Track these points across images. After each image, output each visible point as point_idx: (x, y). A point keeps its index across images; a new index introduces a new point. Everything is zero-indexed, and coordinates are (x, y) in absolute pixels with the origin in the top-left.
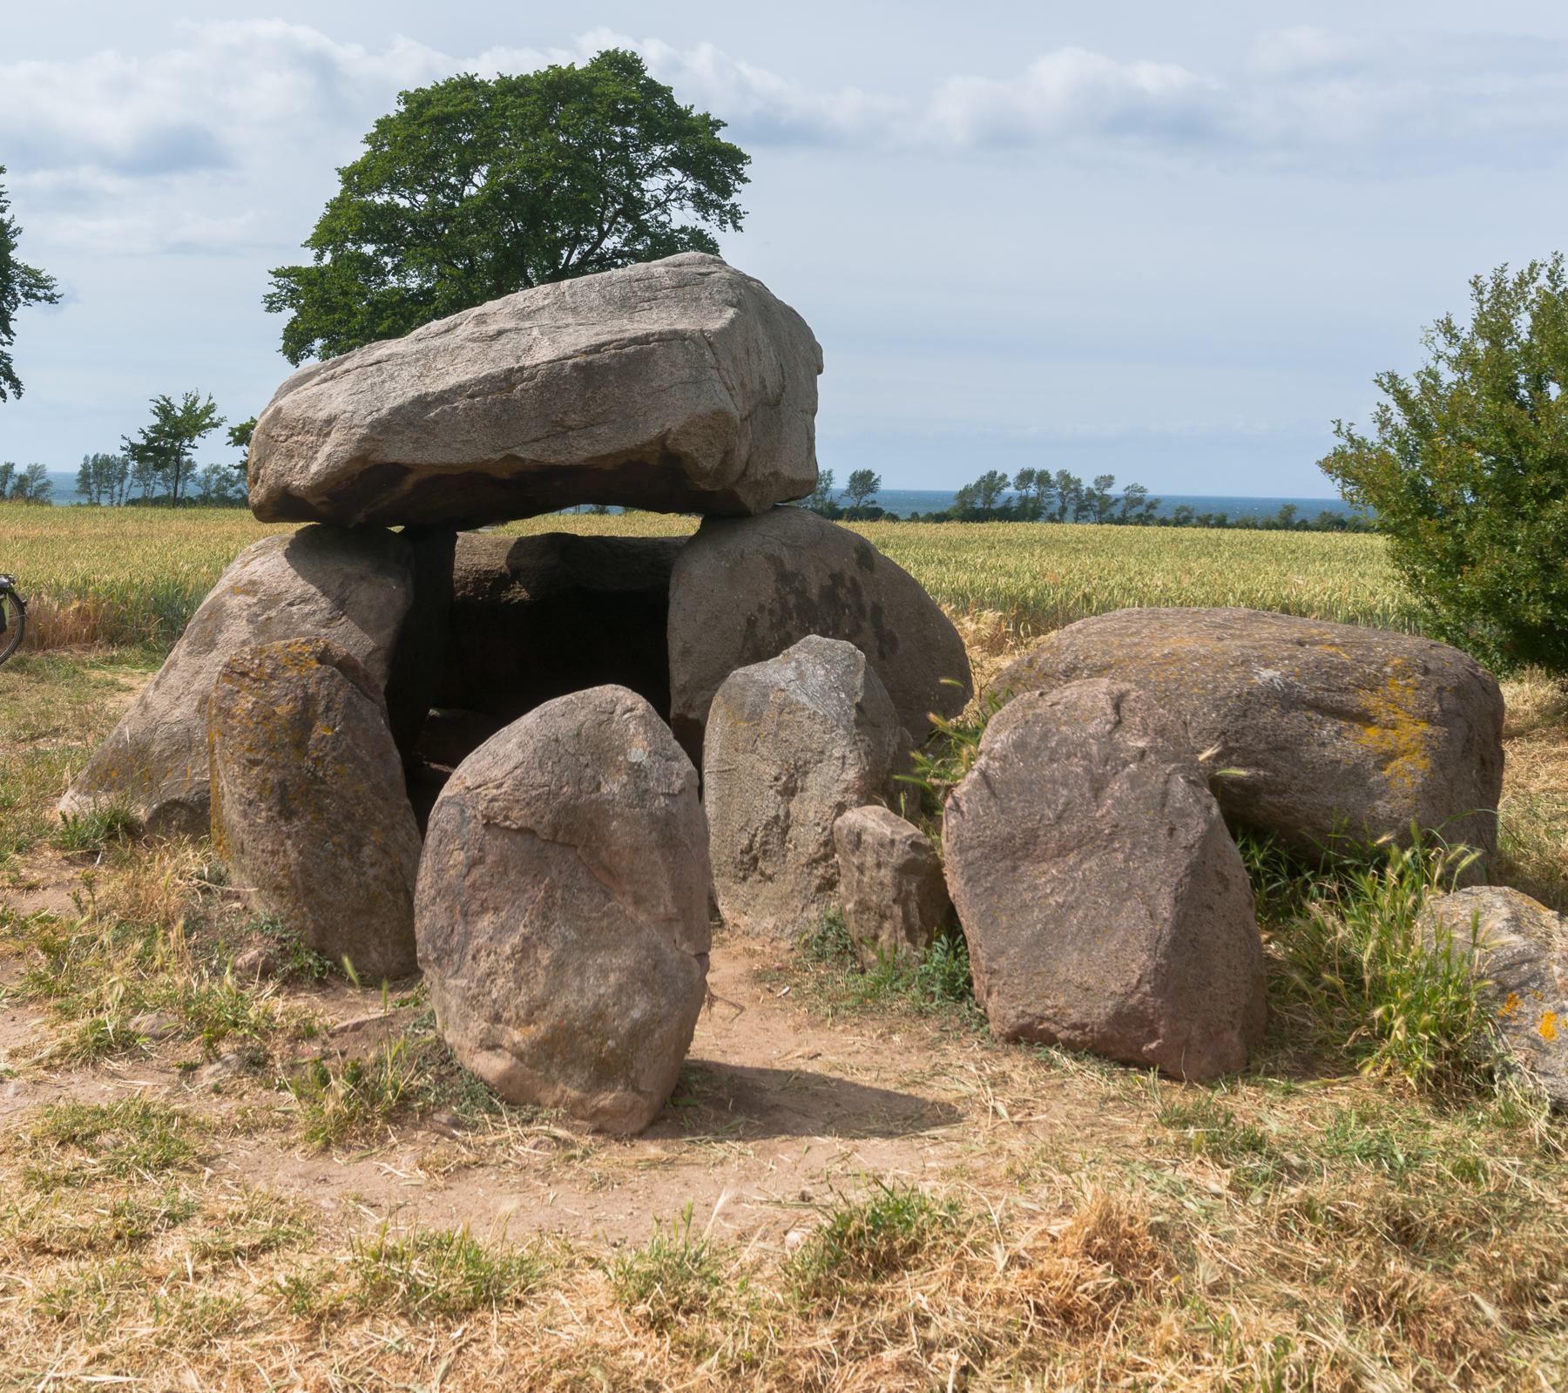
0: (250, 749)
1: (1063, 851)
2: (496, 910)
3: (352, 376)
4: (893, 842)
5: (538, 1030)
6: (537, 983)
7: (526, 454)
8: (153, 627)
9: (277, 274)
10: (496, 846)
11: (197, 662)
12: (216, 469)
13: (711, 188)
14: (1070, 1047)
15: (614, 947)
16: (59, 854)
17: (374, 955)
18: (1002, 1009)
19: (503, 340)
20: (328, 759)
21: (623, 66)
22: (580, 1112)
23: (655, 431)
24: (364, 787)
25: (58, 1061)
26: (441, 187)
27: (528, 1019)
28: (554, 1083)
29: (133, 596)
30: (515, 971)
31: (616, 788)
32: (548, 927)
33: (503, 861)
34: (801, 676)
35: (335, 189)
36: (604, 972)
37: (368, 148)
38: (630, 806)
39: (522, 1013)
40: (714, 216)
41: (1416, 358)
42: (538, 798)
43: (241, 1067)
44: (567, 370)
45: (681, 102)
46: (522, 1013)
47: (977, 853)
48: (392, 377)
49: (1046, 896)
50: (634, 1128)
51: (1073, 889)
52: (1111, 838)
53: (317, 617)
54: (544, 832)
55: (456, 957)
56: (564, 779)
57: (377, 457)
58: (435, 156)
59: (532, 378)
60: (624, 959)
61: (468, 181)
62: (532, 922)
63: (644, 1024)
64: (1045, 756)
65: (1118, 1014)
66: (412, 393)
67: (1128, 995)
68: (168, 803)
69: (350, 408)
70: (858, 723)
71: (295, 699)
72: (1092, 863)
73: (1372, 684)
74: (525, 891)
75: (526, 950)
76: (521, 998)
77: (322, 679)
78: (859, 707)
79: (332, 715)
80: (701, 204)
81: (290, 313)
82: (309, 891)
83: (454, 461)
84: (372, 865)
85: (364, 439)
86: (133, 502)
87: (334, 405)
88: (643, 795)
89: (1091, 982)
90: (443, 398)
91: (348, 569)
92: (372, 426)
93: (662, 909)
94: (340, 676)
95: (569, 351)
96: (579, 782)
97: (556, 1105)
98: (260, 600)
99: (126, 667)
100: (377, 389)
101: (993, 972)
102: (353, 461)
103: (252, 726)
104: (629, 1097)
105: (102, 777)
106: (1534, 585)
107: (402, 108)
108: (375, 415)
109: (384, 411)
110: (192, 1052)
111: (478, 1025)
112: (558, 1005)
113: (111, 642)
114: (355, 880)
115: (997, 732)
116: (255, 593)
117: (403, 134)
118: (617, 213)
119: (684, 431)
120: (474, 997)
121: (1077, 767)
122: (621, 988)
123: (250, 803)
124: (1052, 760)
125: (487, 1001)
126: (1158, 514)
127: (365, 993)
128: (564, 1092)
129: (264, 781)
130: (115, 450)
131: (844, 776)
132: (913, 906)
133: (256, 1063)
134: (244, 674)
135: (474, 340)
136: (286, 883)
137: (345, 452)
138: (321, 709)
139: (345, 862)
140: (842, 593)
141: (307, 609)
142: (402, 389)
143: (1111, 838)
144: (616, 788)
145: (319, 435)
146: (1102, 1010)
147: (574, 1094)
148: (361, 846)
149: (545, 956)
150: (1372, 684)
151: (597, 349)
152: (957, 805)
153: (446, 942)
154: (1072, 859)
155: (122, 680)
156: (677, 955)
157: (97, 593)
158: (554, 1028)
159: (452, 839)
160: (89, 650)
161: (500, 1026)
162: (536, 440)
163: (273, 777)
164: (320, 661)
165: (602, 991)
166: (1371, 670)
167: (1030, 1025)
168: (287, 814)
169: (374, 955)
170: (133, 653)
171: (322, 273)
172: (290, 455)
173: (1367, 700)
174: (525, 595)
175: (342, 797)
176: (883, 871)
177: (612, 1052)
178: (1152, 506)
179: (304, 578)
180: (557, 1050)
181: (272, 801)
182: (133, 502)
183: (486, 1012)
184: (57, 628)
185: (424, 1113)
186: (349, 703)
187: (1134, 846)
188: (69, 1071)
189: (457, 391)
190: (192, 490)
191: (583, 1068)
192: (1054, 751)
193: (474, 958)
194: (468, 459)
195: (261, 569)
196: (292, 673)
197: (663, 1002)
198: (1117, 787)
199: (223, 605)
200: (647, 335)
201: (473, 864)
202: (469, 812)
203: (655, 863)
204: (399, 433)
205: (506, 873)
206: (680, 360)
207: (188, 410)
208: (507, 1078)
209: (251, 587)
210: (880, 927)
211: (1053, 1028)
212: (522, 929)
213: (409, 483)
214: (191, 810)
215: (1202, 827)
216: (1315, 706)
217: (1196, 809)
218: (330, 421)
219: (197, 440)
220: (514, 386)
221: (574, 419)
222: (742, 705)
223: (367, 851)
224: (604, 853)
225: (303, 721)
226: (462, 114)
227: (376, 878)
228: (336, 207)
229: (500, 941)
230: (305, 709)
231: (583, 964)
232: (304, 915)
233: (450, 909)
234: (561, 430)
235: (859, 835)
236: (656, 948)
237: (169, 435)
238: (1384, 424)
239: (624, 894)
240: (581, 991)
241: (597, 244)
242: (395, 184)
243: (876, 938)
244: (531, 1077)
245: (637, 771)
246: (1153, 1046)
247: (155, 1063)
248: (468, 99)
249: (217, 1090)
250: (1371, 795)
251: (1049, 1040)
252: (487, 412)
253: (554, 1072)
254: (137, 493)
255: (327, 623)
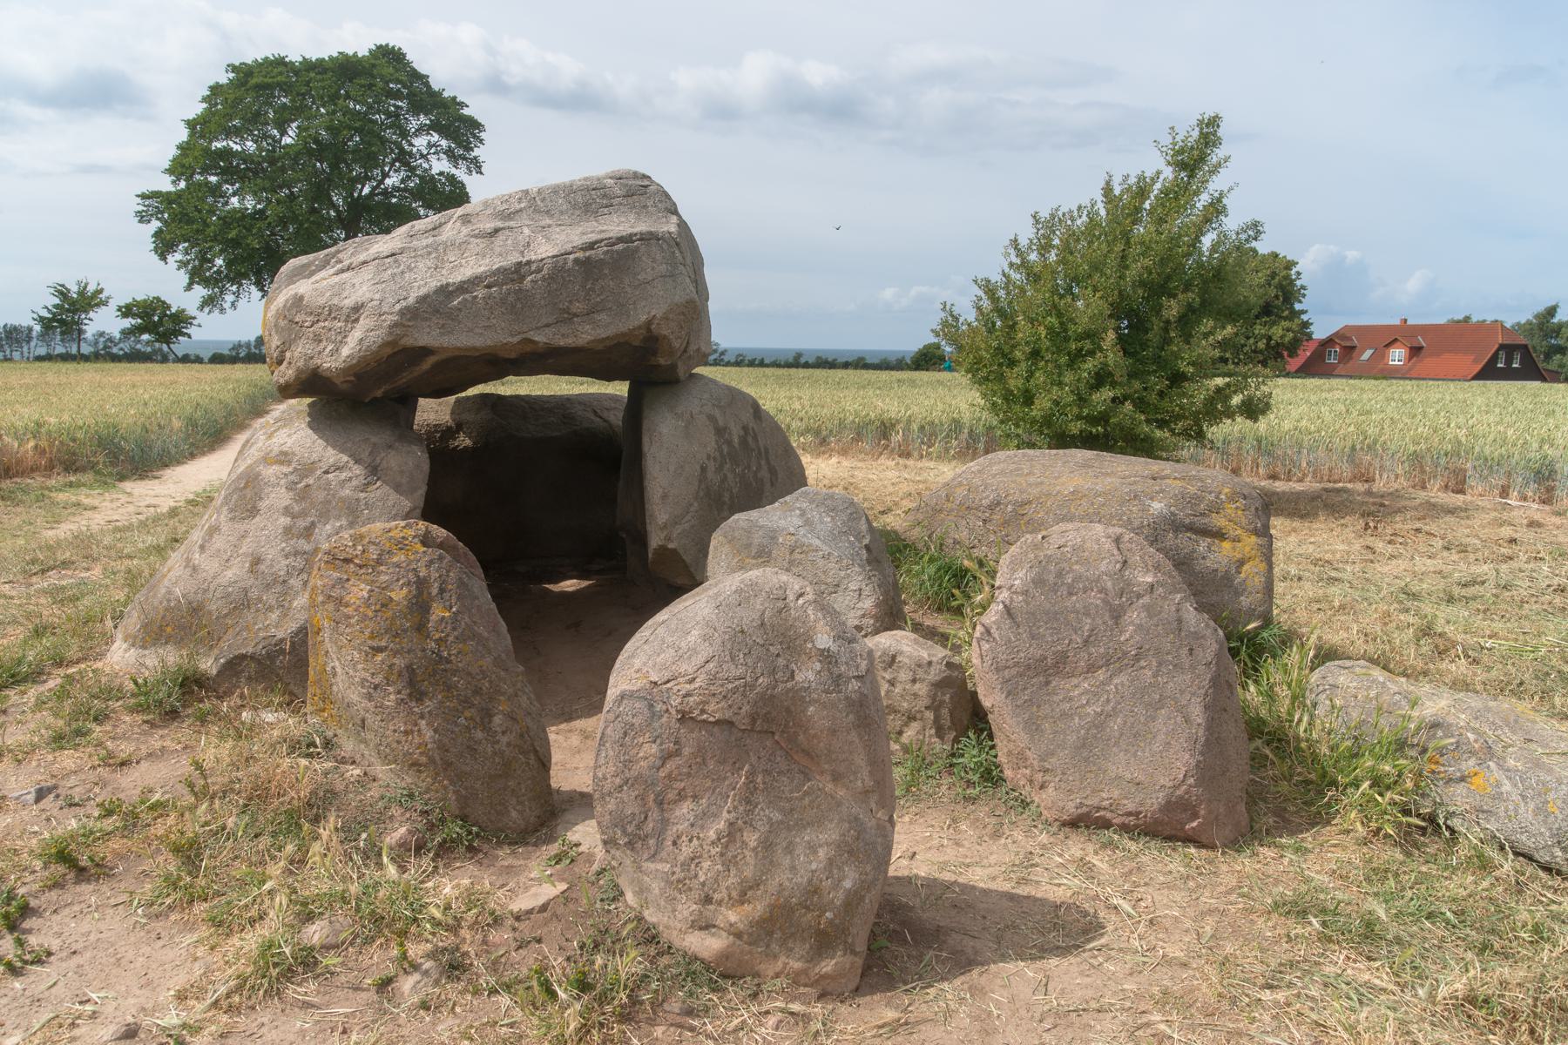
0: (372, 637)
1: (1091, 668)
2: (695, 797)
3: (371, 267)
4: (930, 663)
5: (756, 908)
6: (747, 864)
7: (540, 338)
8: (101, 459)
9: (143, 196)
10: (691, 740)
11: (241, 527)
12: (102, 334)
13: (459, 145)
14: (1125, 828)
15: (818, 823)
16: (139, 718)
17: (514, 814)
18: (1049, 799)
19: (501, 237)
20: (451, 639)
21: (390, 56)
22: (803, 979)
23: (644, 318)
24: (487, 662)
25: (237, 999)
26: (265, 136)
27: (742, 899)
28: (775, 957)
29: (80, 435)
30: (722, 855)
31: (811, 676)
32: (752, 811)
33: (700, 750)
34: (808, 523)
35: (183, 135)
36: (812, 848)
37: (205, 105)
38: (827, 692)
39: (734, 894)
40: (463, 165)
41: (995, 266)
42: (735, 691)
43: (441, 974)
44: (570, 264)
45: (436, 86)
46: (734, 894)
47: (1014, 671)
48: (410, 269)
49: (1083, 706)
50: (852, 986)
51: (1108, 701)
52: (1137, 658)
53: (354, 483)
54: (743, 722)
55: (652, 842)
56: (759, 671)
57: (408, 342)
58: (257, 114)
59: (539, 270)
60: (830, 833)
61: (283, 133)
62: (735, 808)
63: (856, 892)
64: (1064, 591)
65: (1168, 802)
66: (434, 284)
67: (1176, 787)
68: (236, 657)
69: (377, 296)
70: (869, 562)
71: (409, 584)
72: (1122, 679)
73: (1216, 508)
74: (725, 778)
75: (732, 834)
76: (731, 880)
77: (431, 562)
78: (867, 547)
79: (446, 596)
80: (450, 154)
81: (155, 224)
82: (448, 765)
83: (478, 344)
84: (504, 733)
85: (395, 325)
86: (39, 359)
87: (360, 292)
88: (838, 680)
89: (1141, 778)
90: (463, 288)
91: (374, 439)
92: (402, 313)
93: (859, 783)
94: (449, 558)
95: (568, 247)
96: (773, 672)
97: (777, 975)
98: (296, 470)
99: (84, 490)
100: (398, 279)
101: (1046, 771)
102: (385, 344)
103: (371, 614)
104: (849, 958)
105: (153, 634)
106: (1076, 410)
107: (231, 75)
108: (404, 303)
109: (411, 300)
110: (379, 959)
111: (688, 908)
112: (773, 885)
113: (67, 470)
114: (489, 750)
115: (1014, 571)
116: (289, 463)
117: (232, 97)
118: (394, 161)
119: (666, 318)
120: (679, 881)
121: (1095, 598)
122: (831, 861)
123: (376, 687)
124: (1071, 594)
125: (695, 884)
126: (726, 358)
127: (513, 852)
128: (786, 964)
129: (391, 666)
130: (25, 319)
131: (860, 605)
132: (945, 712)
133: (454, 967)
134: (347, 561)
135: (476, 236)
136: (424, 759)
137: (377, 337)
138: (435, 591)
139: (479, 735)
140: (750, 439)
141: (344, 475)
142: (423, 281)
143: (1137, 658)
144: (811, 676)
145: (346, 321)
146: (1153, 802)
147: (797, 965)
148: (491, 716)
149: (752, 839)
150: (1216, 508)
151: (591, 246)
152: (988, 632)
153: (639, 827)
154: (1101, 675)
155: (86, 501)
156: (874, 821)
157: (49, 433)
158: (772, 907)
159: (641, 732)
160: (50, 477)
161: (711, 907)
162: (548, 325)
163: (399, 662)
164: (424, 544)
165: (814, 866)
166: (1212, 497)
167: (1087, 814)
168: (418, 695)
169: (514, 814)
170: (88, 477)
171: (179, 194)
172: (318, 339)
173: (1218, 521)
174: (468, 442)
175: (469, 674)
176: (918, 685)
177: (831, 922)
178: (723, 353)
179: (334, 447)
180: (776, 927)
181: (400, 686)
182: (39, 359)
183: (695, 894)
184: (19, 462)
185: (656, 1005)
186: (462, 584)
187: (1160, 664)
188: (253, 1008)
189: (475, 281)
190: (86, 349)
191: (804, 940)
192: (1070, 586)
193: (675, 843)
194: (489, 343)
195: (290, 442)
196: (399, 557)
197: (868, 868)
198: (1134, 616)
199: (259, 474)
200: (631, 235)
201: (666, 757)
202: (659, 707)
203: (852, 743)
204: (426, 319)
205: (704, 762)
206: (658, 257)
207: (82, 293)
208: (725, 956)
209: (284, 458)
210: (906, 725)
211: (1109, 815)
212: (725, 814)
213: (431, 361)
214: (259, 662)
215: (1215, 646)
216: (1190, 528)
217: (1208, 632)
218: (357, 309)
219: (91, 314)
220: (523, 278)
221: (578, 307)
222: (749, 546)
223: (497, 720)
224: (801, 737)
225: (420, 605)
226: (278, 84)
227: (509, 744)
228: (184, 148)
229: (702, 827)
230: (420, 593)
231: (791, 843)
232: (445, 788)
233: (642, 798)
234: (567, 317)
235: (894, 657)
236: (856, 819)
237: (68, 311)
238: (979, 308)
239: (822, 773)
240: (793, 868)
241: (382, 182)
242: (229, 133)
243: (900, 733)
244: (750, 952)
245: (826, 656)
246: (1194, 824)
247: (343, 978)
248: (281, 73)
249: (425, 1006)
250: (1237, 594)
251: (1106, 824)
252: (503, 301)
253: (775, 947)
254: (42, 351)
255: (364, 488)
